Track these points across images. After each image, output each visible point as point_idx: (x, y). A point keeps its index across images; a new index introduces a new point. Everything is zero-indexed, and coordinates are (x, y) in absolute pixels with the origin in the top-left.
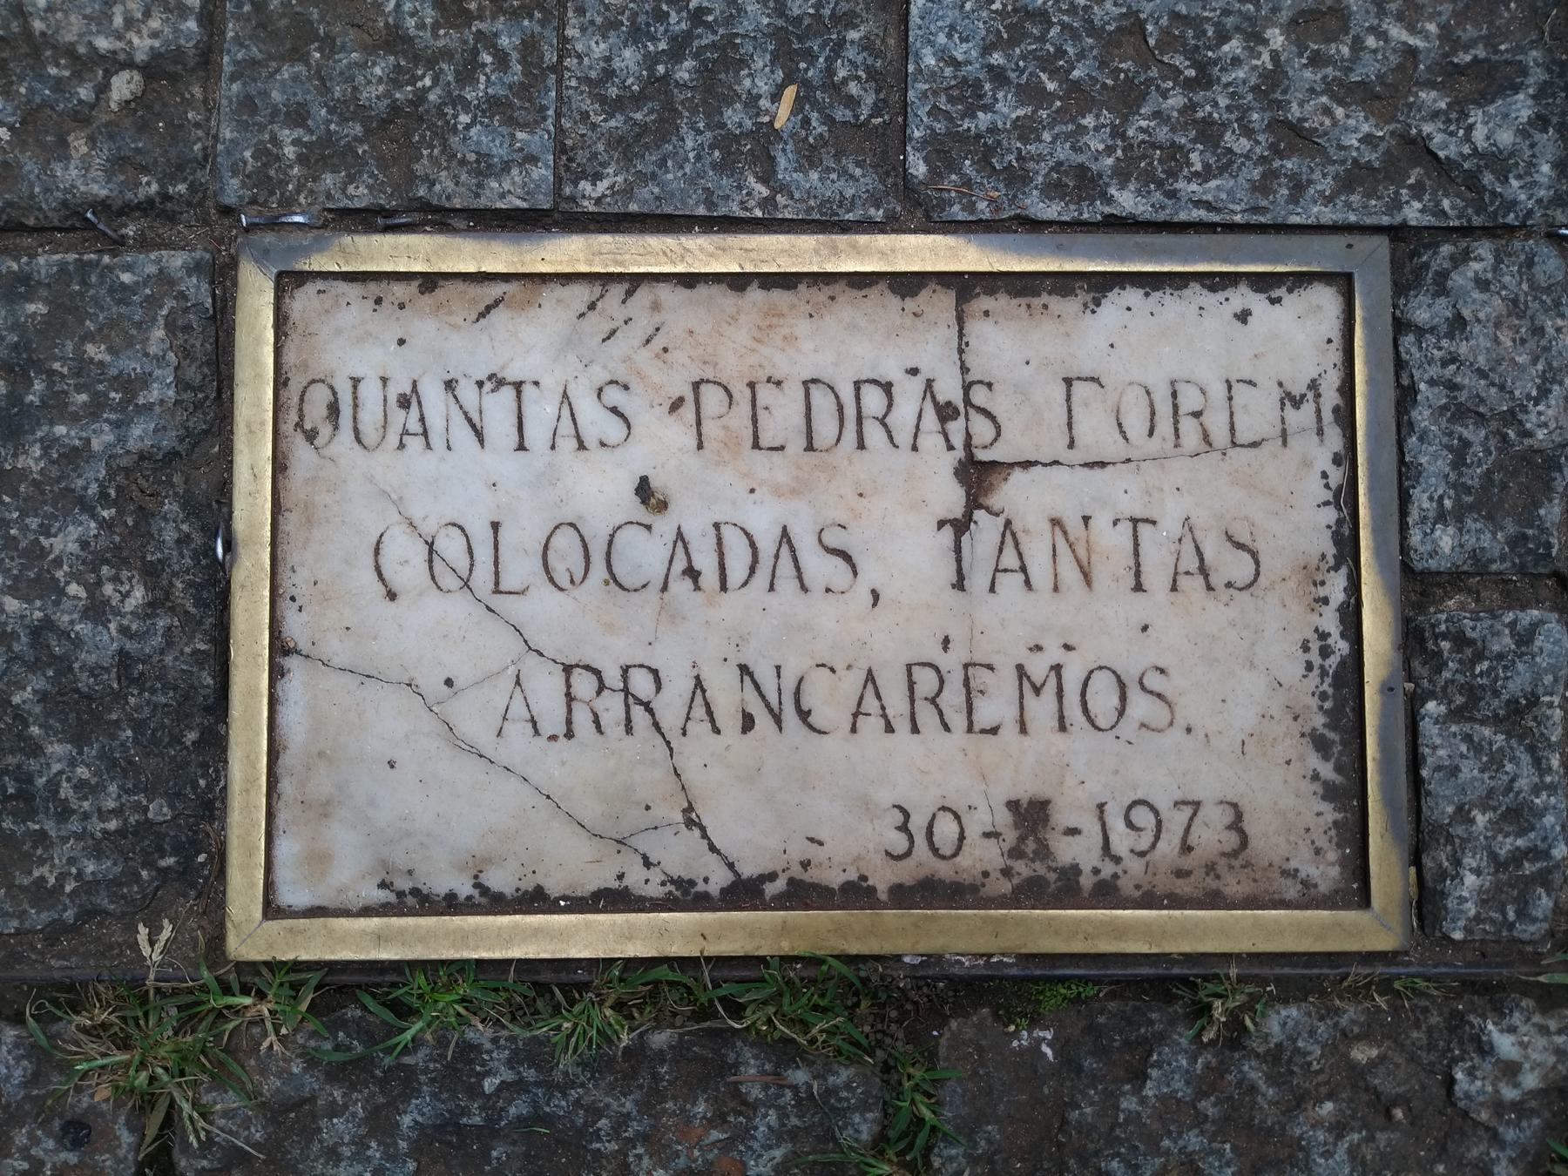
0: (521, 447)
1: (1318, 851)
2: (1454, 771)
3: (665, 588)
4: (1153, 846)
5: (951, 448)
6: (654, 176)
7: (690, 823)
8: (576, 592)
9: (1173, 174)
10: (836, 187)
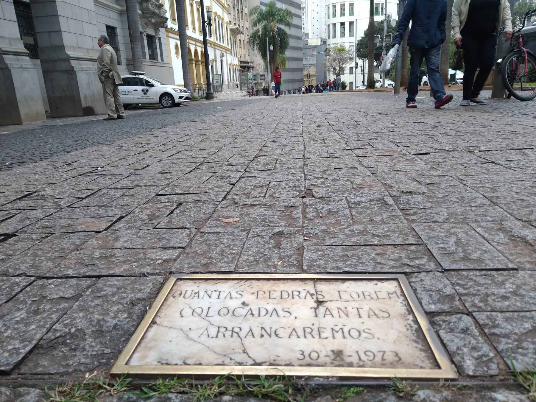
1: (423, 361)
2: (453, 341)
4: (374, 359)
7: (244, 352)
8: (226, 317)
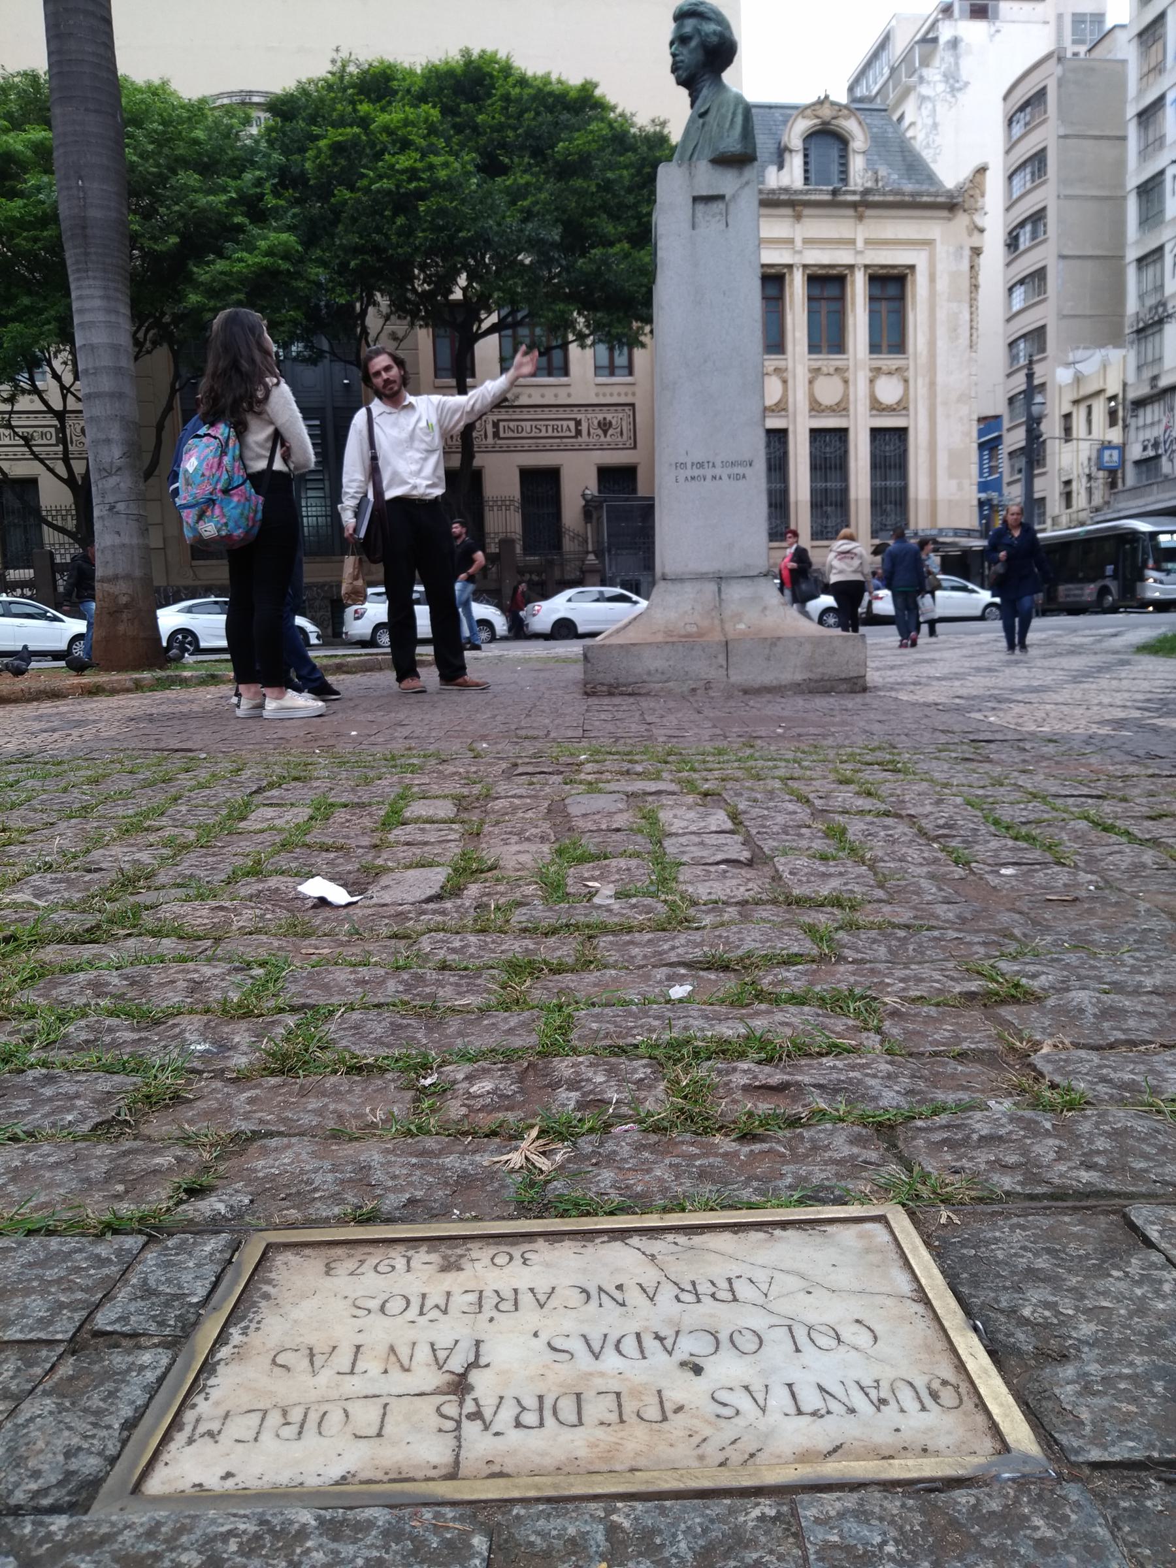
0: (790, 1386)
3: (677, 1333)
5: (475, 1400)
6: (712, 1521)
9: (257, 1537)
10: (553, 1526)
